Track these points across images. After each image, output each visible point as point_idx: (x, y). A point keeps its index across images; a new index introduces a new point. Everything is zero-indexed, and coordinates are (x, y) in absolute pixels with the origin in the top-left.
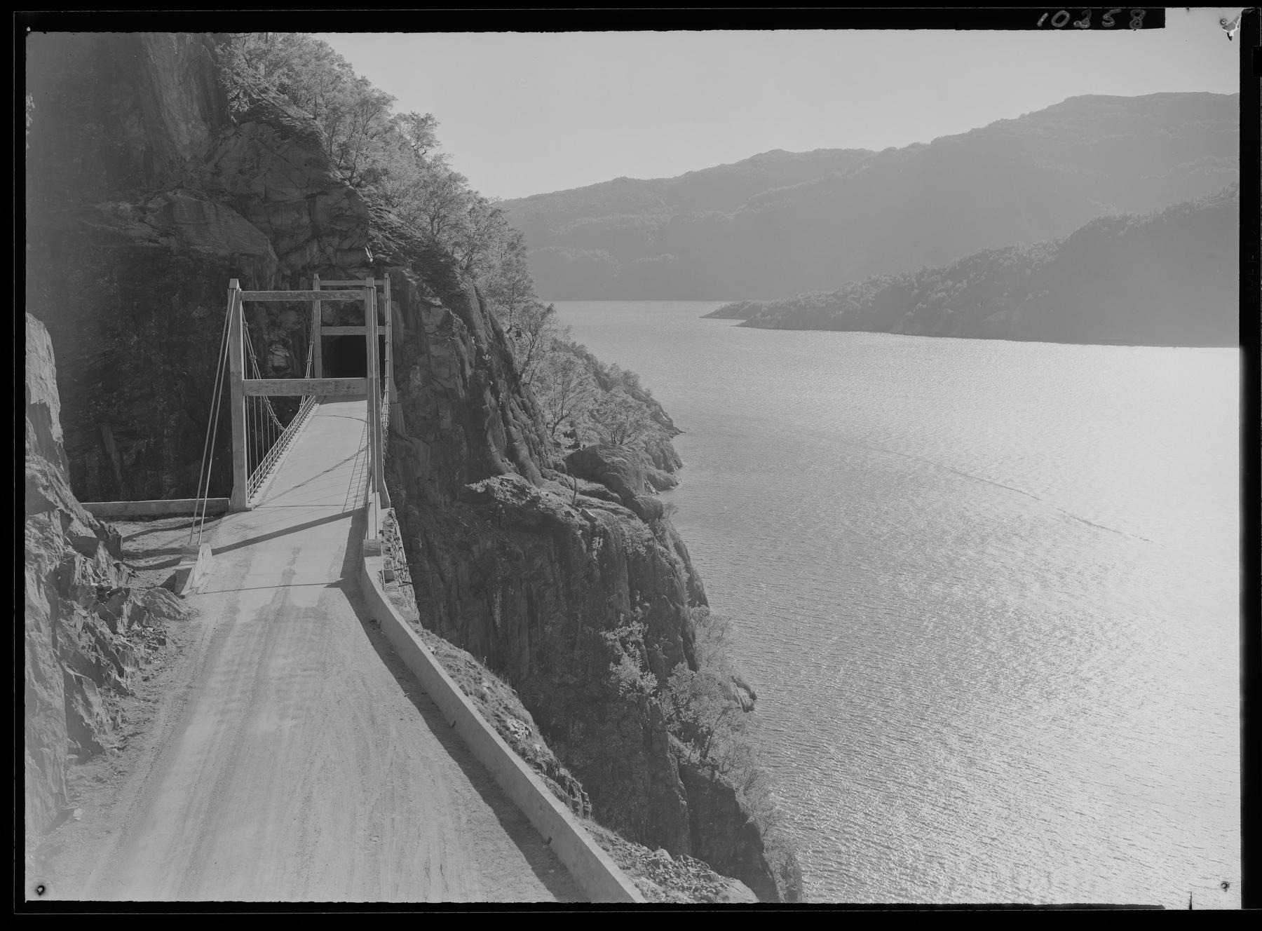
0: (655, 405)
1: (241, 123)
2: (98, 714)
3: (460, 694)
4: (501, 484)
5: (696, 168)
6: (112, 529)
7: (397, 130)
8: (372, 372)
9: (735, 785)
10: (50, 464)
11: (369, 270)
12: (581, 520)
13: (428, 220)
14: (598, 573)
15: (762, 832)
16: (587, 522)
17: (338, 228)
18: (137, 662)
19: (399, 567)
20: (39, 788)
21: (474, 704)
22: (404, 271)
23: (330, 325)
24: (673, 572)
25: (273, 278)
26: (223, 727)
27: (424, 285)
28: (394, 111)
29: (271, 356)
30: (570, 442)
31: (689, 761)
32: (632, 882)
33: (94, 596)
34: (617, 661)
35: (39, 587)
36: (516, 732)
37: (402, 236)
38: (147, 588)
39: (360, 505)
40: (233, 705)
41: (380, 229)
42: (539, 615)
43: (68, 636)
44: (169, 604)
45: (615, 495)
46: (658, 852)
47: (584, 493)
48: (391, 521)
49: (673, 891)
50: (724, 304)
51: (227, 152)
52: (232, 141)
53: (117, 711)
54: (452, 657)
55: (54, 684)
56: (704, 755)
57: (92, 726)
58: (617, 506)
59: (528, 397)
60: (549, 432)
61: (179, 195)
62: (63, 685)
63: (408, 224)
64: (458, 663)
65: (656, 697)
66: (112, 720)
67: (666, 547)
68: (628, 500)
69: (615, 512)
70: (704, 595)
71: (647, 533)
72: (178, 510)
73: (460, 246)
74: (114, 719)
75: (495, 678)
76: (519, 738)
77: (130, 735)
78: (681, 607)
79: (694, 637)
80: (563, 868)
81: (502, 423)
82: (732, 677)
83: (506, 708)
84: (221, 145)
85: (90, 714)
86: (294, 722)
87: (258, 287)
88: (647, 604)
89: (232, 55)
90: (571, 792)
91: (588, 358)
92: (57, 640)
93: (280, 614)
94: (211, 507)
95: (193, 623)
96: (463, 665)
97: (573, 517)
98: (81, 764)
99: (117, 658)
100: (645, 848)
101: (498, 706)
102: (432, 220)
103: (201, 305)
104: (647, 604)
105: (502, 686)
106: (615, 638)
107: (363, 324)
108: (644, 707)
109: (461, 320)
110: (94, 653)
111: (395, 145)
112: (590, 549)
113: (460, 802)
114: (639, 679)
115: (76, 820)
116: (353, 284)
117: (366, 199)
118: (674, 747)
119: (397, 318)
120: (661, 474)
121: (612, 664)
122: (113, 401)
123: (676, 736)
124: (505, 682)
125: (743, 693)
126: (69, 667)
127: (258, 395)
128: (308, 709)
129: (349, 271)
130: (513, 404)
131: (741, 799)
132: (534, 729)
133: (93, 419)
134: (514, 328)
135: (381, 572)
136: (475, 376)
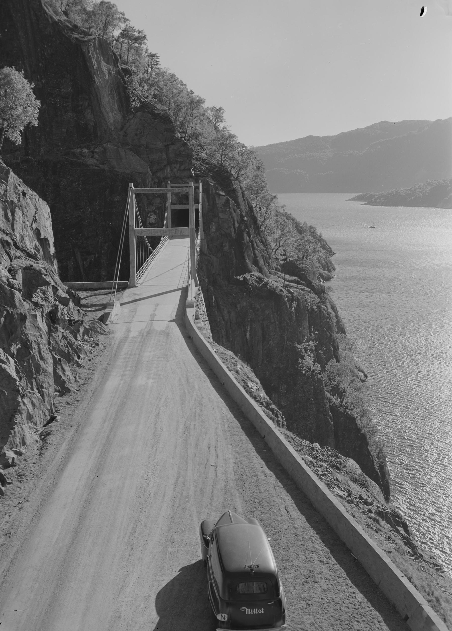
0: (323, 241)
1: (136, 113)
2: (68, 375)
3: (226, 370)
4: (251, 277)
5: (345, 131)
6: (76, 294)
7: (207, 115)
8: (191, 224)
9: (355, 416)
10: (49, 265)
11: (192, 179)
12: (287, 293)
13: (220, 156)
14: (294, 318)
15: (368, 437)
16: (290, 295)
17: (179, 160)
18: (86, 353)
19: (202, 313)
20: (42, 407)
21: (233, 375)
22: (208, 179)
23: (175, 204)
24: (329, 317)
25: (150, 183)
26: (122, 382)
27: (217, 185)
28: (205, 106)
29: (149, 218)
30: (284, 258)
31: (334, 404)
32: (301, 457)
33: (67, 323)
34: (303, 358)
35: (42, 319)
36: (252, 388)
37: (207, 163)
38: (91, 320)
39: (185, 285)
40: (127, 373)
41: (198, 160)
42: (267, 336)
43: (55, 341)
44: (101, 328)
45: (303, 282)
46: (314, 444)
47: (289, 281)
48: (199, 292)
49: (320, 462)
50: (357, 195)
51: (130, 126)
52: (132, 121)
53: (77, 374)
54: (224, 354)
55: (48, 362)
56: (341, 402)
57: (66, 380)
58: (304, 287)
59: (264, 237)
60: (274, 253)
61: (109, 146)
62: (52, 362)
63: (210, 158)
64: (226, 356)
65: (320, 375)
66: (74, 378)
67: (326, 307)
68: (309, 284)
69: (303, 290)
70: (344, 329)
71: (318, 300)
72: (106, 286)
73: (234, 168)
74: (75, 377)
75: (243, 364)
76: (253, 391)
77: (82, 385)
78: (332, 334)
79: (338, 348)
80: (270, 450)
81: (251, 249)
82: (356, 367)
83: (248, 377)
84: (127, 122)
85: (65, 375)
86: (153, 381)
87: (143, 187)
88: (317, 332)
89: (132, 81)
90: (277, 416)
91: (293, 219)
92: (51, 342)
93: (149, 333)
94: (120, 285)
95: (111, 336)
96: (229, 357)
97: (283, 292)
98: (61, 397)
99: (77, 351)
100: (308, 442)
101: (244, 376)
102: (221, 156)
103: (118, 195)
104: (317, 332)
105: (246, 367)
106: (301, 347)
107: (188, 204)
108: (315, 379)
109: (233, 202)
110: (67, 348)
111: (205, 122)
112: (291, 307)
113: (225, 418)
114: (312, 366)
115: (57, 421)
116: (185, 186)
117: (191, 147)
118: (328, 397)
119: (205, 201)
120: (325, 273)
121: (300, 359)
122: (80, 238)
123: (329, 392)
124: (248, 365)
125: (361, 374)
126: (56, 354)
127: (141, 235)
128: (160, 375)
129: (184, 180)
130: (257, 240)
131: (358, 422)
132: (260, 387)
133: (71, 246)
134: (258, 205)
135: (193, 315)
136: (239, 227)
